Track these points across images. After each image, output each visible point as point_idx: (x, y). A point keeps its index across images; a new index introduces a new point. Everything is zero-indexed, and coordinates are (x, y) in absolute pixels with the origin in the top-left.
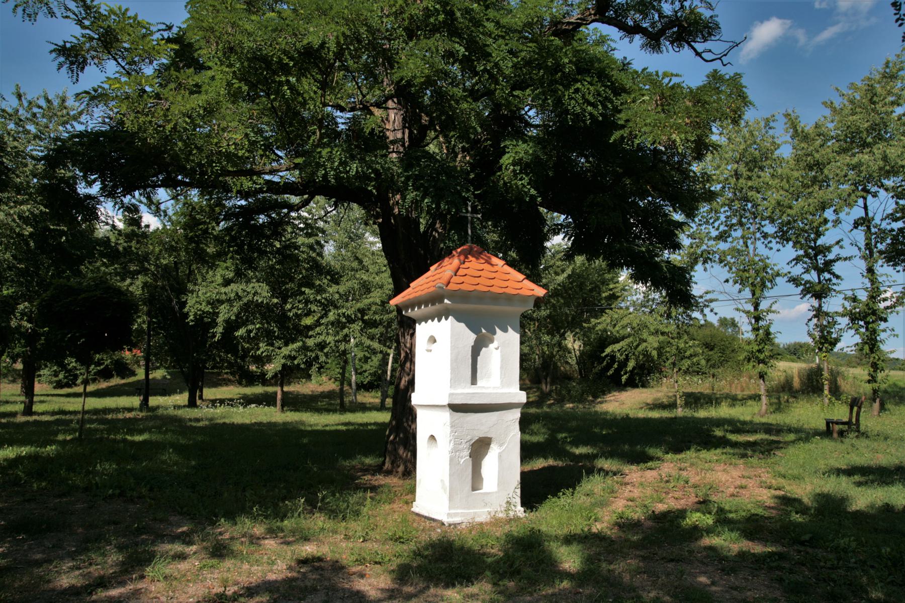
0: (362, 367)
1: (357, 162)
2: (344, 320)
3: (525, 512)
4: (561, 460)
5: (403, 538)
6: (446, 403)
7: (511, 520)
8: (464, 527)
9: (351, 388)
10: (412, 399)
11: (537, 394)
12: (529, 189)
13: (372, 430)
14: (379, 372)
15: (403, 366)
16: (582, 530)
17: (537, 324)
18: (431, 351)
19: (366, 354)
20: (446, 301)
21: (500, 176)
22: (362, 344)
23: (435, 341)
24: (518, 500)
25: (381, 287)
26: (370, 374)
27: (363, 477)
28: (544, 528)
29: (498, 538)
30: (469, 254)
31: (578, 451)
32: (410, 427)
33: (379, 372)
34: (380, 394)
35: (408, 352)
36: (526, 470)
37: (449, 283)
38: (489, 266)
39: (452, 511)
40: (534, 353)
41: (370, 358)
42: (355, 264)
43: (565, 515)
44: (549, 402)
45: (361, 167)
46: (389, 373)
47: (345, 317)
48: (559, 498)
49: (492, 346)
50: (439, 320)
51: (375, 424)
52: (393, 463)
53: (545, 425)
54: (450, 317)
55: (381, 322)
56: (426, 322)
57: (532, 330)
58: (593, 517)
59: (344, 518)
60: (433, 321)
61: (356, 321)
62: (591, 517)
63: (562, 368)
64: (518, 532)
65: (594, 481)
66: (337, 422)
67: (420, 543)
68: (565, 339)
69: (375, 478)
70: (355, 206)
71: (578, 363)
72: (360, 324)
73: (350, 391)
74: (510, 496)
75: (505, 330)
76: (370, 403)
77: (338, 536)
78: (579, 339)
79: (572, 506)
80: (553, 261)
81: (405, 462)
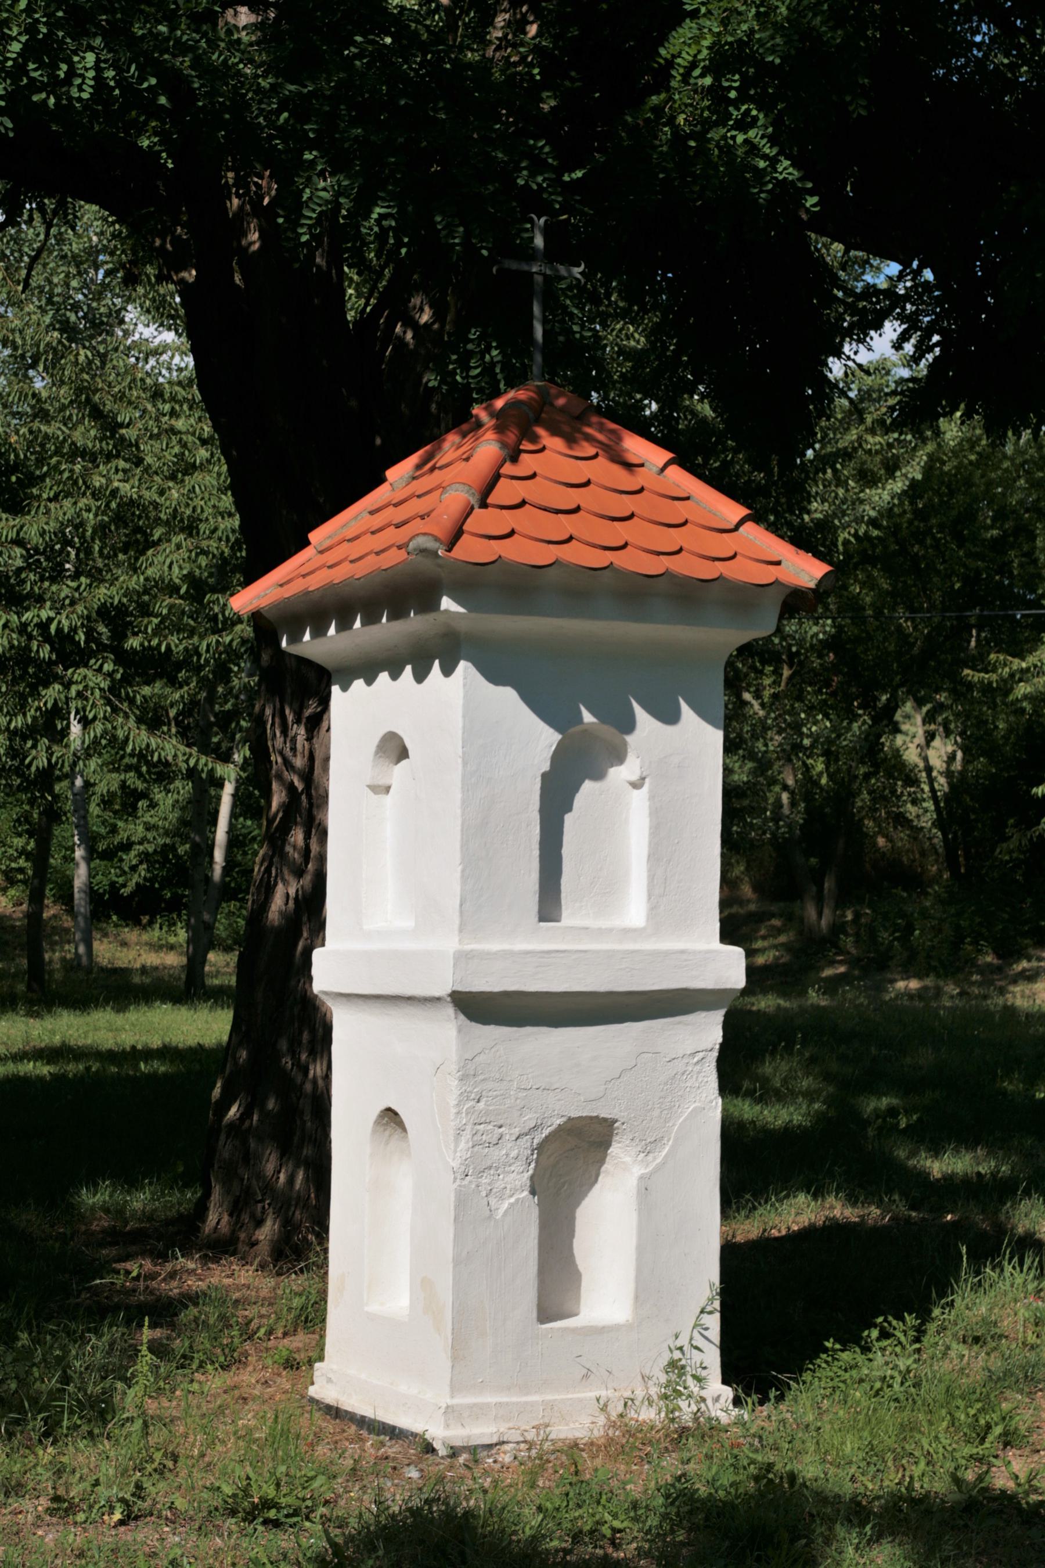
0: (114, 830)
1: (98, 41)
2: (45, 652)
3: (737, 1402)
4: (873, 1196)
5: (277, 1506)
6: (443, 989)
7: (683, 1431)
8: (507, 1459)
9: (71, 910)
10: (315, 971)
11: (782, 939)
12: (774, 161)
13: (153, 1076)
14: (183, 849)
15: (277, 839)
16: (957, 1481)
17: (786, 672)
18: (387, 789)
19: (131, 778)
20: (447, 603)
21: (658, 110)
22: (117, 744)
23: (403, 754)
24: (712, 1358)
25: (191, 528)
26: (145, 857)
27: (121, 1266)
28: (809, 1469)
29: (635, 1505)
30: (538, 421)
31: (937, 1167)
32: (305, 1071)
33: (183, 849)
34: (182, 935)
35: (299, 785)
36: (740, 1239)
37: (457, 534)
38: (617, 470)
39: (459, 1400)
40: (773, 781)
41: (144, 795)
42: (85, 435)
43: (891, 1418)
44: (828, 972)
45: (115, 66)
46: (219, 855)
47: (47, 638)
48: (866, 1349)
49: (621, 774)
50: (420, 676)
51: (167, 1052)
52: (235, 1210)
53: (813, 1060)
54: (463, 665)
55: (190, 660)
56: (369, 682)
57: (767, 693)
58: (998, 1430)
59: (50, 1433)
60: (395, 676)
61: (92, 654)
62: (988, 1427)
63: (881, 841)
64: (711, 1482)
65: (1003, 1286)
66: (18, 1046)
67: (342, 1524)
68: (896, 730)
69: (169, 1267)
70: (90, 212)
71: (940, 823)
72: (108, 667)
73: (67, 922)
74: (683, 1341)
75: (671, 717)
76: (144, 970)
77: (27, 1504)
78: (948, 733)
79: (917, 1385)
80: (853, 435)
81: (284, 1204)
